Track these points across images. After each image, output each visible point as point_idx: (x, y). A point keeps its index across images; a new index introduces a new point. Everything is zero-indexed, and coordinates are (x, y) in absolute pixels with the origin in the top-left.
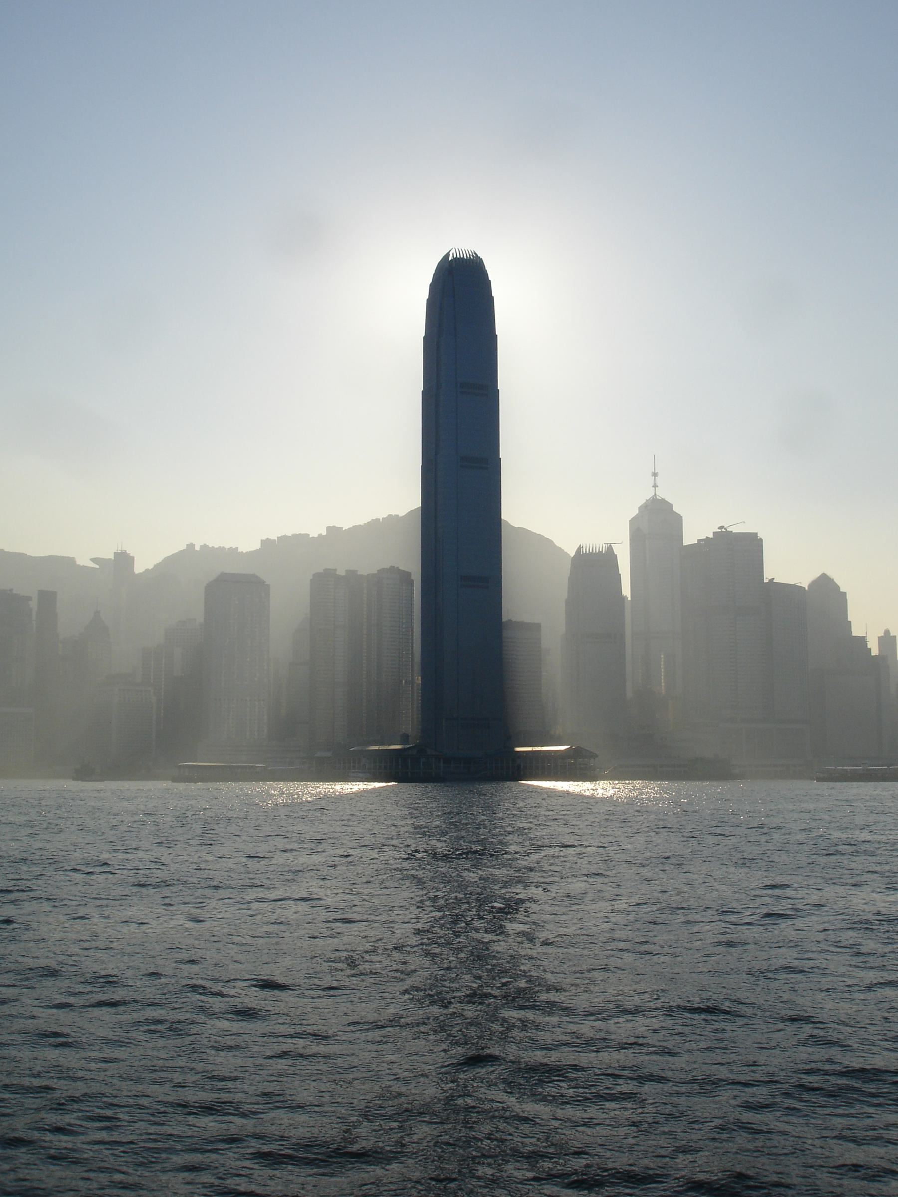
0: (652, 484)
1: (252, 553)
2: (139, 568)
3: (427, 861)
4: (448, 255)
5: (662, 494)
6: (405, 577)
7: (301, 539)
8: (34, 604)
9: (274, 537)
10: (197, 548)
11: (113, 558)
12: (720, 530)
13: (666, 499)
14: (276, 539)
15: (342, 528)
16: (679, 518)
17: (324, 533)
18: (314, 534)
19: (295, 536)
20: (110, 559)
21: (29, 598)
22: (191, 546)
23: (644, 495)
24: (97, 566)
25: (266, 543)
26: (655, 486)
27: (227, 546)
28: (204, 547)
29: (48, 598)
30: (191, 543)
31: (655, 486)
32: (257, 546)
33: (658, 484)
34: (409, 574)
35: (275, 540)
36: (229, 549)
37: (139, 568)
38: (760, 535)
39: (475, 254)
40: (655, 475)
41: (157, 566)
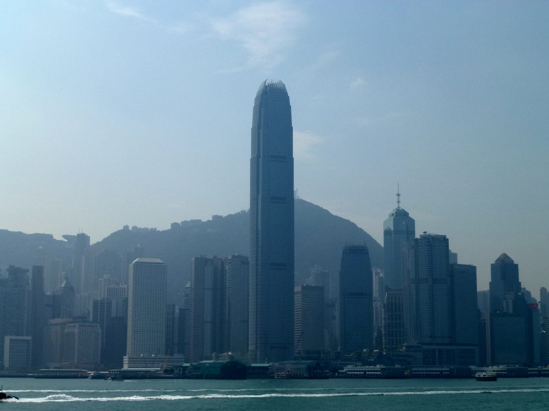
0: (397, 201)
1: (164, 232)
2: (93, 242)
3: (122, 309)
4: (265, 83)
5: (403, 206)
6: (245, 262)
7: (197, 223)
8: (30, 274)
9: (179, 222)
10: (130, 229)
11: (77, 235)
12: (424, 234)
13: (405, 210)
14: (180, 223)
15: (222, 216)
16: (412, 221)
17: (211, 219)
18: (204, 220)
19: (192, 221)
20: (75, 236)
21: (28, 271)
22: (126, 227)
23: (391, 209)
24: (66, 241)
25: (174, 225)
26: (399, 202)
27: (150, 227)
28: (135, 228)
29: (38, 271)
30: (127, 226)
31: (399, 202)
32: (169, 227)
33: (400, 201)
34: (247, 258)
35: (179, 224)
36: (150, 229)
37: (93, 242)
38: (447, 237)
39: (281, 81)
40: (398, 195)
41: (105, 240)
